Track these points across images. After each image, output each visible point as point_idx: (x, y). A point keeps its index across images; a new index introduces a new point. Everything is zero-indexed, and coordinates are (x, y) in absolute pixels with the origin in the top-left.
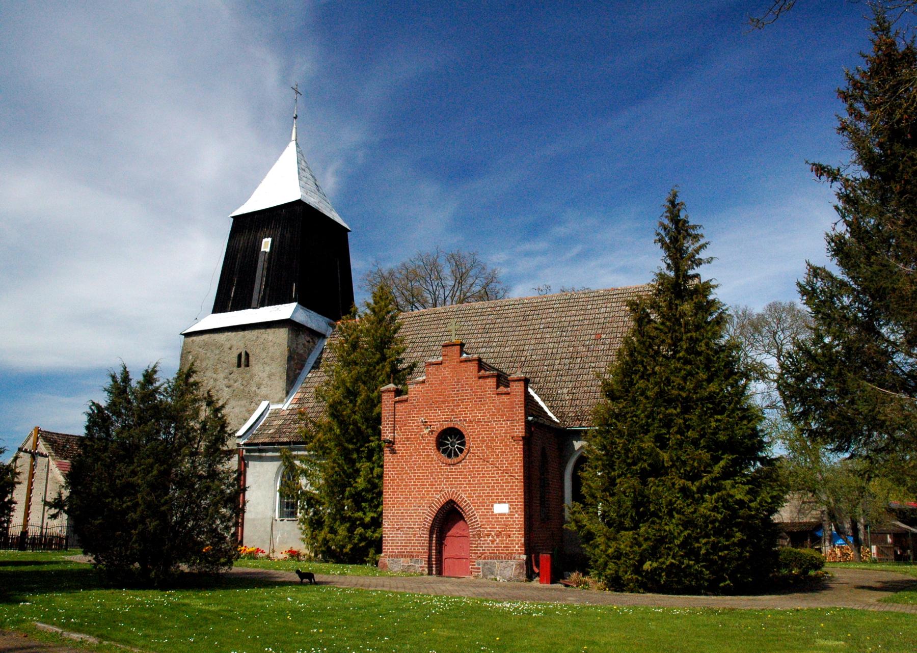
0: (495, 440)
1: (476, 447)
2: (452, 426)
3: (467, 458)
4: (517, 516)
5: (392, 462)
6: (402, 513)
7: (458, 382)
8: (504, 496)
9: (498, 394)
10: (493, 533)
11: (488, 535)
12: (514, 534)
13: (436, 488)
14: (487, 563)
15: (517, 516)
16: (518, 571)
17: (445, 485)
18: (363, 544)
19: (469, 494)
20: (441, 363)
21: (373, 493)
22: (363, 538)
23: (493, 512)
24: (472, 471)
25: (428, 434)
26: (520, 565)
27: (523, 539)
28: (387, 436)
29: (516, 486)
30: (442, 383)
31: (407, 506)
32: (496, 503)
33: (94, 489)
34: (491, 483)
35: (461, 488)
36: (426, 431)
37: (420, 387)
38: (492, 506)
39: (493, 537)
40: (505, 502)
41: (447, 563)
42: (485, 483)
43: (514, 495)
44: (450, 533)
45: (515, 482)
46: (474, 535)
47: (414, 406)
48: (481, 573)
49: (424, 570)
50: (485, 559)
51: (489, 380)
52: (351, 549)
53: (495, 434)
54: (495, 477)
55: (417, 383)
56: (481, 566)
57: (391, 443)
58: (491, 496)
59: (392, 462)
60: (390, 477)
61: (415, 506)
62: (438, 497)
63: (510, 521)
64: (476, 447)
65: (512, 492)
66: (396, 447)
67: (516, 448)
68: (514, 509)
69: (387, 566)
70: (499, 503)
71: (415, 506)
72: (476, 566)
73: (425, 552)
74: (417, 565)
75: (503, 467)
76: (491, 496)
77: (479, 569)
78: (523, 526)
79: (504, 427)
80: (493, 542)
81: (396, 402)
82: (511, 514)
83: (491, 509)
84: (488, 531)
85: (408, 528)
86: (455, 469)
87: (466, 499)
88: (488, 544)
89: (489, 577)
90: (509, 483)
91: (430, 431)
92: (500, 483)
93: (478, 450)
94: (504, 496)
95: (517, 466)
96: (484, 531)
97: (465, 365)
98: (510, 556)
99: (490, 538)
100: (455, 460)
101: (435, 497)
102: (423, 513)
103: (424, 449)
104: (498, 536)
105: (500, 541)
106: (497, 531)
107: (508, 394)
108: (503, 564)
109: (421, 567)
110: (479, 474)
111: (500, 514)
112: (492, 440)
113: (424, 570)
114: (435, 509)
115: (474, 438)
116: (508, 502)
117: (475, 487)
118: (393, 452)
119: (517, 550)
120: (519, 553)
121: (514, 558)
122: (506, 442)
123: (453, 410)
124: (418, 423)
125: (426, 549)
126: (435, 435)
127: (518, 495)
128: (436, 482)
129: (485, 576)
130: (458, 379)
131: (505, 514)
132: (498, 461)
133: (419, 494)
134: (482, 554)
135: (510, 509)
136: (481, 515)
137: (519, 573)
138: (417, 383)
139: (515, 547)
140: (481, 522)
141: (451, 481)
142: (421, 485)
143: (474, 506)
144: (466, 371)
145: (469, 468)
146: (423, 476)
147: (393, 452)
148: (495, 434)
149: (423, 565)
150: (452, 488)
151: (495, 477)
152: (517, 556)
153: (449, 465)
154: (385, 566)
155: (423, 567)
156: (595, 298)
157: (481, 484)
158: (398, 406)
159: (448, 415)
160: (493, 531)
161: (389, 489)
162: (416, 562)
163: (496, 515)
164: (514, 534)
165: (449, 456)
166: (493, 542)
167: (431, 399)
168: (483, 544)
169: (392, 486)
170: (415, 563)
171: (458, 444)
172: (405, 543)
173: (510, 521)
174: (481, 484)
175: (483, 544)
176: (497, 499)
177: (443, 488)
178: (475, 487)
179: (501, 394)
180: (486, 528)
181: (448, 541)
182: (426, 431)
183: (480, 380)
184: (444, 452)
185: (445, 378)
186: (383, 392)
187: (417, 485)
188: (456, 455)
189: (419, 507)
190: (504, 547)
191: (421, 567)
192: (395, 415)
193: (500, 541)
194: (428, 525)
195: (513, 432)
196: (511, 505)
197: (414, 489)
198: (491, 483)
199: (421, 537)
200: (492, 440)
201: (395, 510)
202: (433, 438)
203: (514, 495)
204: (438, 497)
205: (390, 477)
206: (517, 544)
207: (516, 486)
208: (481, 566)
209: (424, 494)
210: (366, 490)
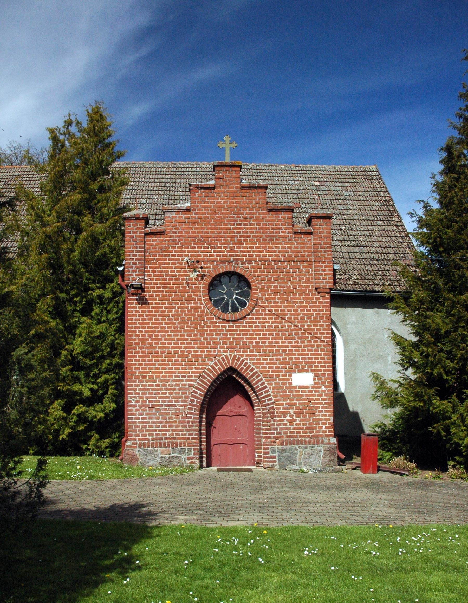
0: (292, 291)
1: (266, 299)
2: (232, 269)
3: (254, 312)
4: (323, 388)
5: (140, 316)
6: (158, 385)
7: (239, 213)
8: (306, 363)
9: (296, 233)
10: (292, 412)
11: (285, 414)
12: (320, 412)
13: (209, 352)
14: (285, 450)
15: (323, 388)
16: (328, 458)
17: (221, 347)
18: (82, 427)
19: (258, 359)
20: (214, 188)
21: (93, 358)
22: (82, 418)
23: (291, 384)
24: (261, 331)
25: (197, 279)
26: (330, 451)
27: (332, 418)
28: (134, 279)
29: (322, 350)
30: (215, 214)
31: (164, 377)
32: (294, 371)
33: (27, 415)
34: (287, 346)
35: (245, 351)
36: (193, 275)
37: (183, 216)
38: (290, 376)
39: (291, 416)
40: (307, 371)
41: (215, 450)
42: (279, 347)
43: (319, 363)
44: (221, 412)
45: (320, 346)
46: (264, 414)
47: (173, 240)
48: (277, 463)
49: (194, 463)
50: (282, 444)
51: (283, 214)
52: (69, 435)
53: (292, 283)
54: (294, 338)
55: (178, 211)
56: (276, 455)
57: (141, 288)
58: (289, 363)
59: (140, 316)
60: (137, 336)
61: (177, 376)
62: (212, 363)
63: (314, 395)
64: (266, 299)
65: (317, 359)
66: (147, 295)
67: (321, 303)
68: (319, 379)
69: (137, 460)
70: (300, 372)
71: (177, 376)
72: (270, 454)
73: (193, 439)
74: (183, 456)
75: (304, 326)
76: (289, 363)
77: (274, 457)
78: (331, 401)
79: (305, 275)
80: (291, 422)
81: (146, 234)
82: (316, 387)
83: (288, 380)
84: (284, 408)
85: (166, 405)
86: (236, 327)
87: (252, 366)
88: (285, 425)
89: (288, 468)
90: (313, 346)
91: (198, 276)
92: (301, 346)
93: (268, 303)
94: (306, 363)
95: (322, 326)
96: (278, 409)
97: (248, 192)
98: (316, 440)
99: (288, 418)
100: (230, 316)
101: (208, 364)
102: (190, 385)
103: (190, 299)
104: (298, 414)
105: (301, 420)
106: (297, 408)
107: (311, 233)
108: (308, 450)
109: (189, 459)
110: (270, 334)
111: (301, 387)
112: (289, 291)
113: (194, 463)
114: (209, 379)
115: (263, 287)
116: (312, 371)
117: (265, 351)
118: (143, 301)
119: (324, 432)
120: (327, 436)
121: (322, 442)
122: (308, 295)
123: (232, 249)
124: (181, 263)
125: (195, 434)
126: (207, 280)
127: (325, 362)
128: (209, 343)
129: (282, 467)
130: (239, 210)
131: (307, 387)
132: (297, 318)
133: (183, 360)
134: (277, 438)
135: (314, 379)
136: (274, 388)
137: (330, 461)
138: (178, 211)
139: (321, 428)
140: (275, 396)
141: (231, 343)
142: (185, 348)
143: (265, 376)
144: (250, 201)
145: (257, 326)
146: (188, 335)
147: (143, 301)
148: (292, 283)
149: (192, 455)
150: (232, 352)
151: (294, 338)
152: (326, 440)
153: (228, 321)
154: (134, 459)
155: (192, 458)
156: (278, 171)
157: (274, 347)
158: (151, 240)
159: (226, 255)
160: (292, 408)
161: (138, 352)
162: (182, 452)
163: (295, 387)
164: (320, 412)
165: (225, 310)
166: (291, 422)
167: (199, 233)
168: (278, 425)
169: (141, 348)
170: (180, 453)
171: (237, 294)
172: (163, 426)
173: (314, 395)
174: (274, 347)
175: (278, 425)
176: (296, 367)
177: (219, 351)
178: (265, 351)
179: (300, 233)
180: (282, 404)
181: (218, 422)
182: (193, 275)
183: (271, 214)
184: (216, 303)
185: (219, 208)
186: (125, 219)
187: (180, 348)
188: (235, 310)
189: (184, 377)
190: (307, 428)
191: (189, 459)
192: (145, 252)
193: (301, 420)
194: (197, 402)
195: (319, 282)
196: (316, 375)
197: (175, 352)
198: (287, 346)
199: (186, 418)
200: (289, 291)
201: (147, 381)
202: (203, 286)
203: (319, 363)
204: (212, 363)
205: (137, 336)
206: (324, 424)
207: (322, 350)
208: (276, 455)
209: (191, 360)
210: (85, 354)
